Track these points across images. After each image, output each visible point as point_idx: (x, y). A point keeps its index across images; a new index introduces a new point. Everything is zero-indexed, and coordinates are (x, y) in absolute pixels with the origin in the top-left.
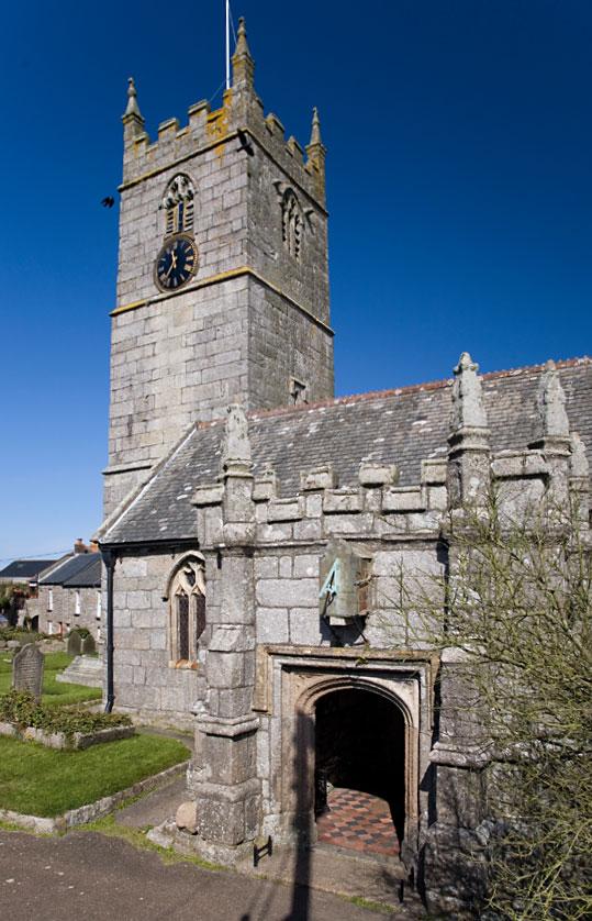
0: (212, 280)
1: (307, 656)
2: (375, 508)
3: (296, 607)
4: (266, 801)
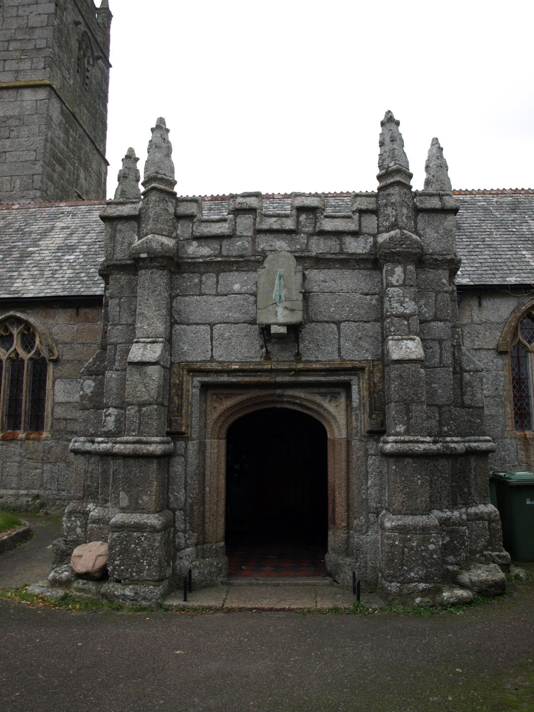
0: (11, 84)
1: (235, 371)
3: (220, 323)
4: (180, 534)
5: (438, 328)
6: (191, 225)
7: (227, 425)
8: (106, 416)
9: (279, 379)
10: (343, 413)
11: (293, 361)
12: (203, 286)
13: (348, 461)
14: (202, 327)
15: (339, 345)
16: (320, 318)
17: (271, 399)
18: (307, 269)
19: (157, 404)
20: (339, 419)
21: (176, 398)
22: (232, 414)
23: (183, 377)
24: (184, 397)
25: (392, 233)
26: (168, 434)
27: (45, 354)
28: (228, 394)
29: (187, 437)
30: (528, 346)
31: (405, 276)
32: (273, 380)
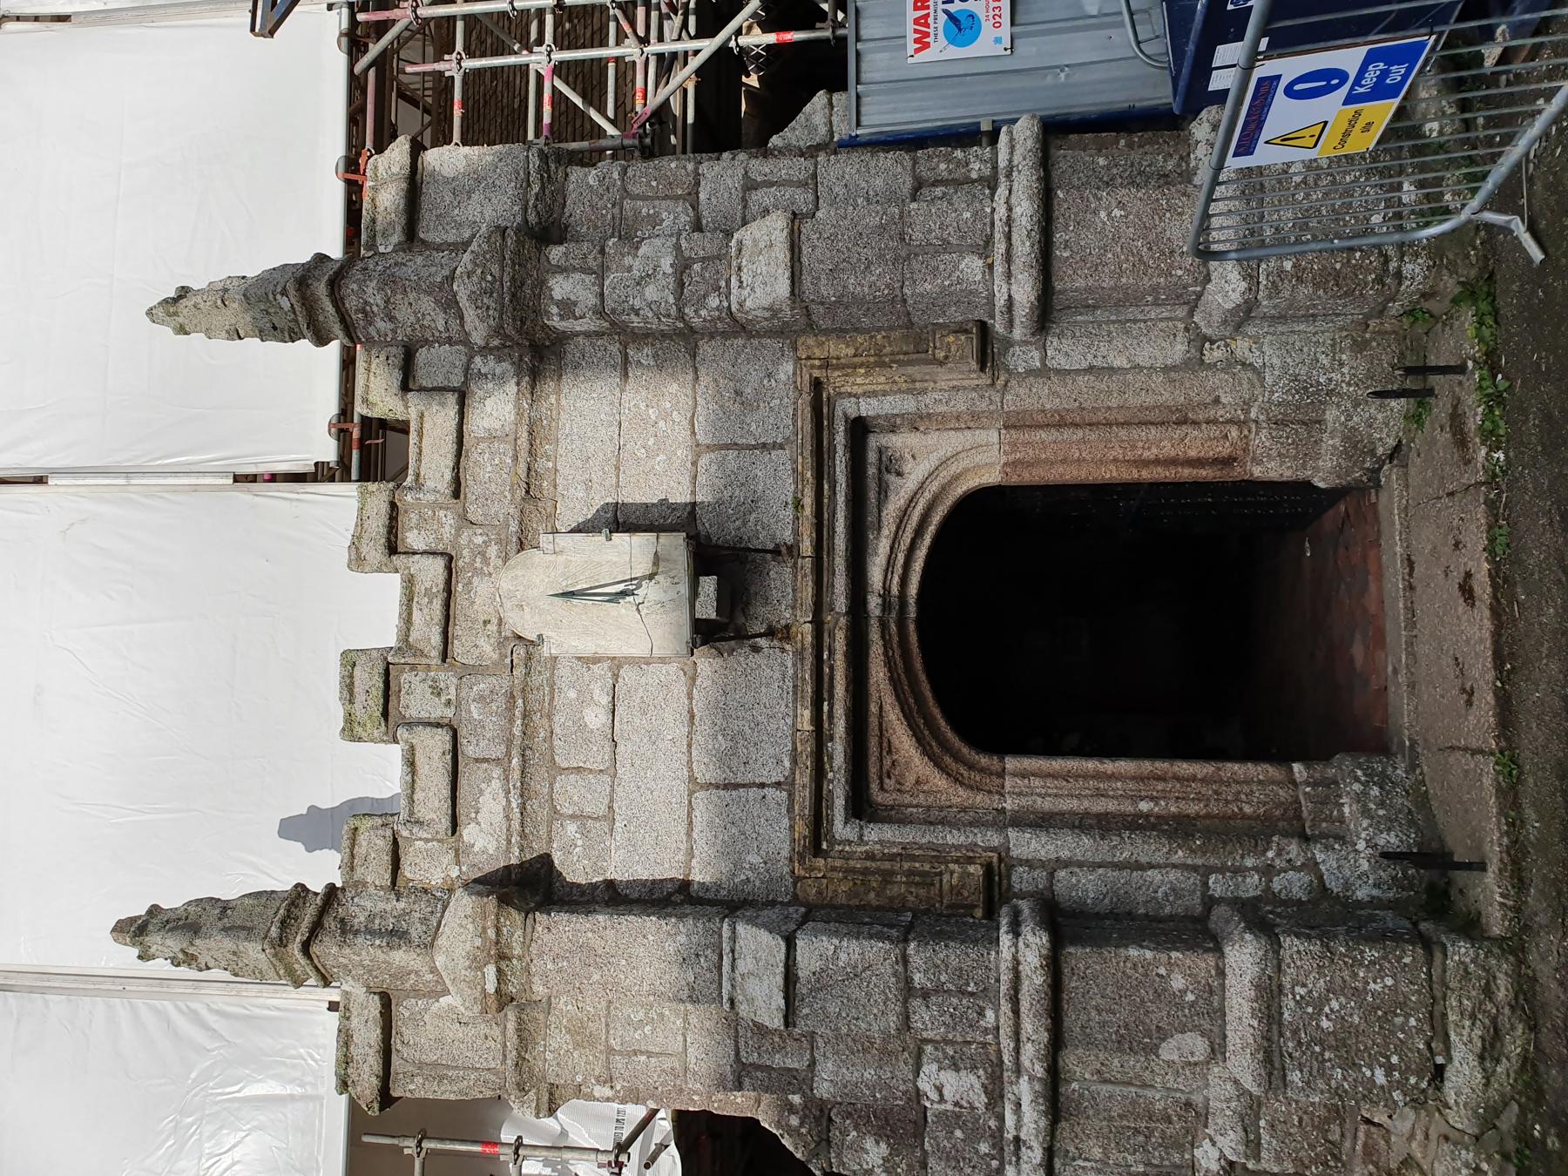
8: (942, 1100)
10: (933, 438)
11: (795, 565)
12: (588, 810)
13: (1061, 422)
15: (755, 447)
17: (893, 627)
19: (906, 941)
20: (949, 450)
25: (463, 301)
26: (991, 913)
28: (881, 744)
29: (1000, 860)
31: (575, 269)
32: (843, 621)
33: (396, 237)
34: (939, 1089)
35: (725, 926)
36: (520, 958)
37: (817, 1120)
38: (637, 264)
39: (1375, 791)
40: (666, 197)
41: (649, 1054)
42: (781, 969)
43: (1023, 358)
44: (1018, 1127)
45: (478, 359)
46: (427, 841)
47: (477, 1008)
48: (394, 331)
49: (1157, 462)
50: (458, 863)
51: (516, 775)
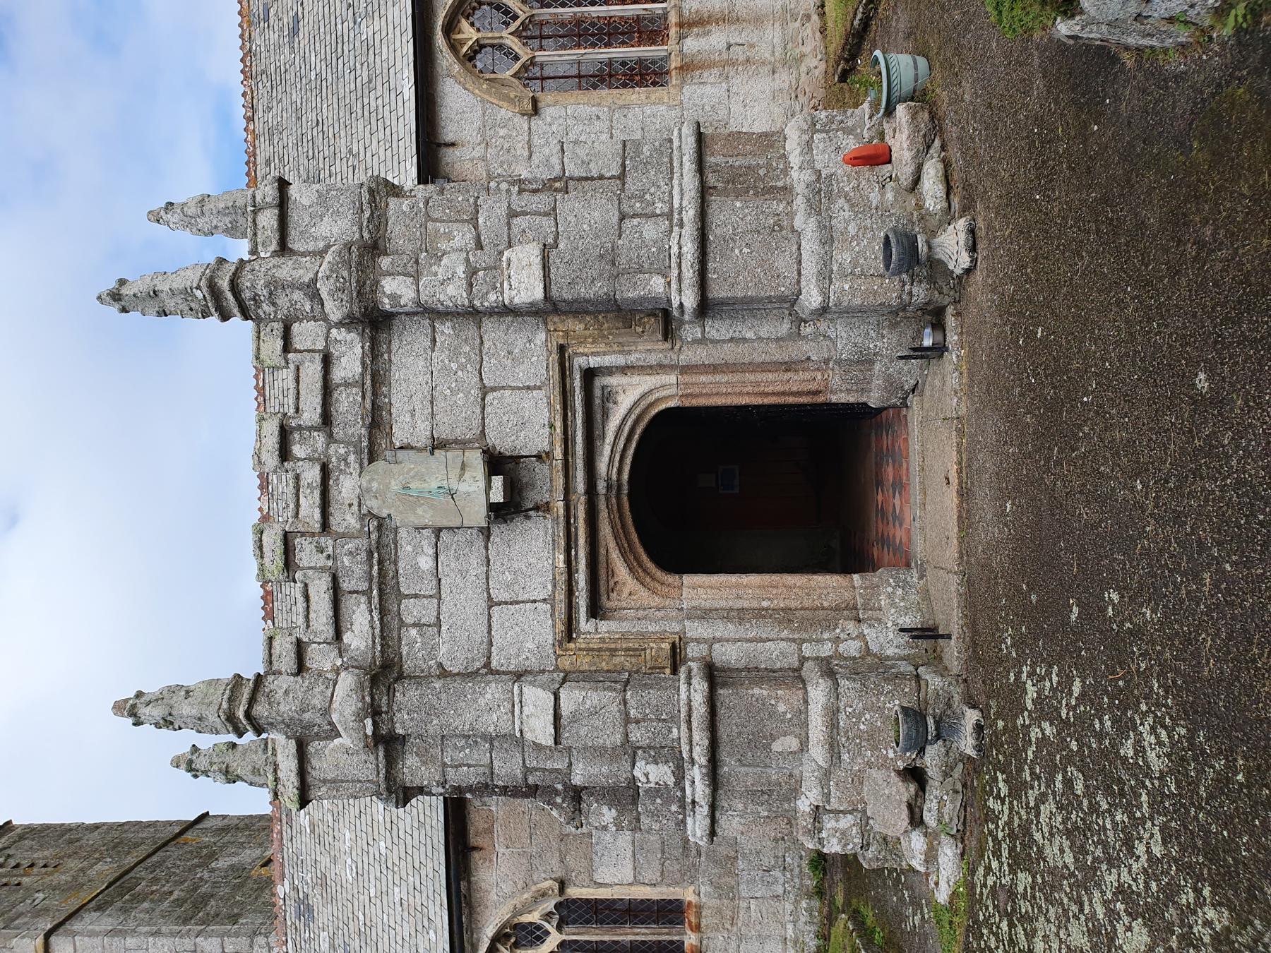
1: (568, 561)
2: (320, 439)
5: (491, 215)
6: (314, 645)
7: (658, 573)
8: (648, 782)
9: (581, 487)
10: (636, 379)
12: (423, 621)
13: (714, 368)
14: (494, 619)
16: (476, 423)
17: (614, 500)
18: (391, 442)
21: (617, 660)
22: (641, 566)
23: (580, 649)
24: (613, 646)
25: (324, 295)
26: (675, 671)
27: (549, 905)
30: (523, 60)
31: (399, 274)
32: (583, 499)
33: (274, 246)
34: (646, 775)
35: (516, 687)
36: (387, 713)
37: (573, 798)
38: (440, 270)
39: (900, 591)
40: (456, 221)
41: (469, 766)
42: (552, 712)
43: (691, 332)
44: (693, 795)
45: (334, 331)
46: (319, 643)
47: (361, 745)
48: (276, 312)
49: (774, 394)
50: (341, 656)
51: (376, 600)
